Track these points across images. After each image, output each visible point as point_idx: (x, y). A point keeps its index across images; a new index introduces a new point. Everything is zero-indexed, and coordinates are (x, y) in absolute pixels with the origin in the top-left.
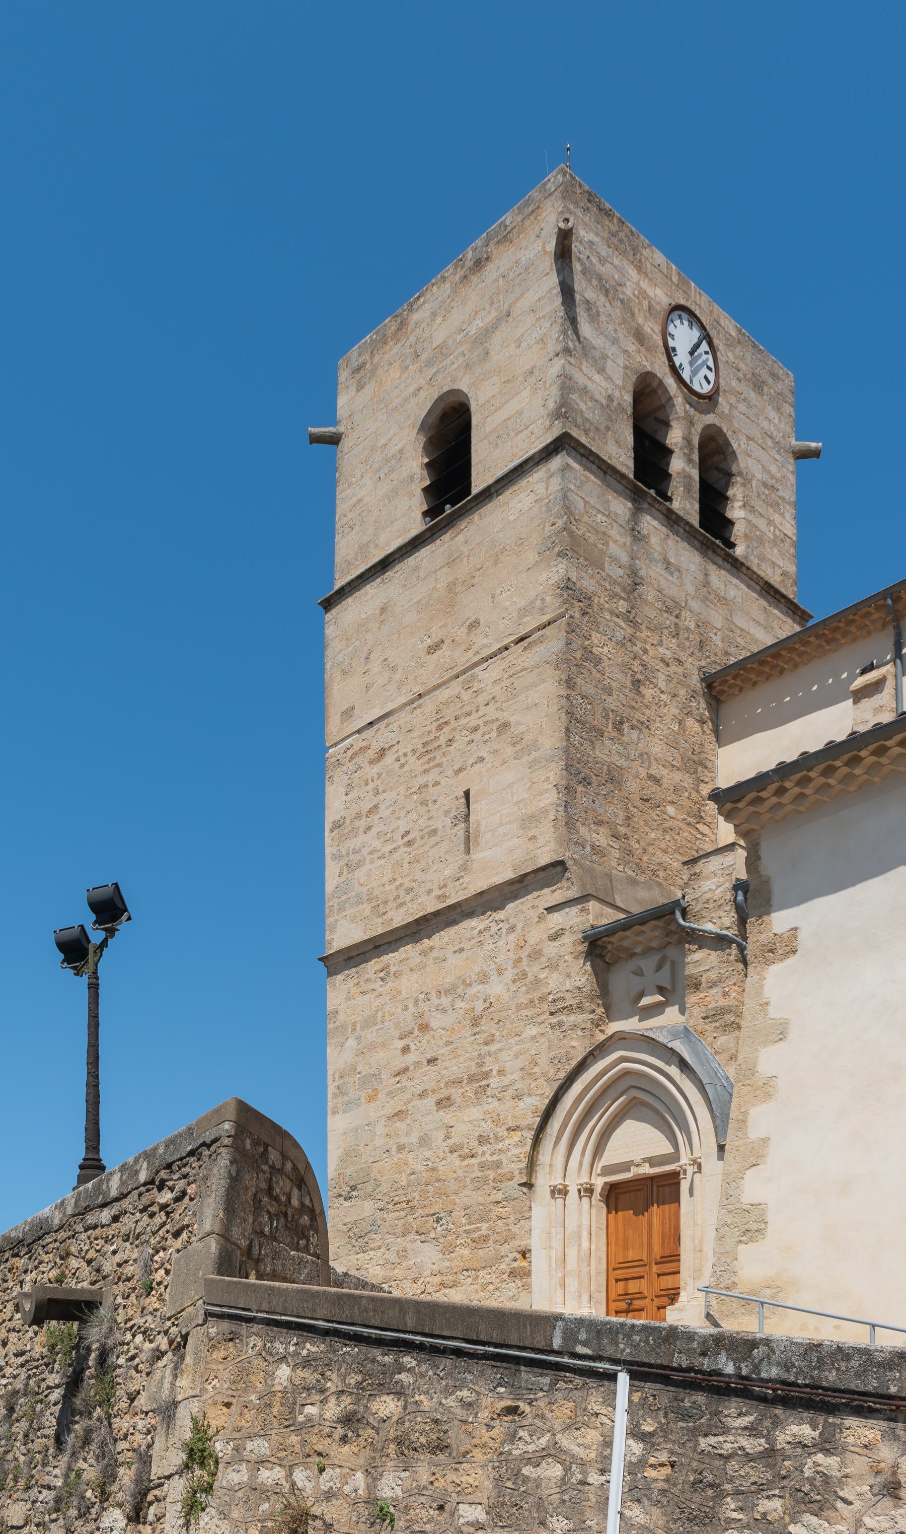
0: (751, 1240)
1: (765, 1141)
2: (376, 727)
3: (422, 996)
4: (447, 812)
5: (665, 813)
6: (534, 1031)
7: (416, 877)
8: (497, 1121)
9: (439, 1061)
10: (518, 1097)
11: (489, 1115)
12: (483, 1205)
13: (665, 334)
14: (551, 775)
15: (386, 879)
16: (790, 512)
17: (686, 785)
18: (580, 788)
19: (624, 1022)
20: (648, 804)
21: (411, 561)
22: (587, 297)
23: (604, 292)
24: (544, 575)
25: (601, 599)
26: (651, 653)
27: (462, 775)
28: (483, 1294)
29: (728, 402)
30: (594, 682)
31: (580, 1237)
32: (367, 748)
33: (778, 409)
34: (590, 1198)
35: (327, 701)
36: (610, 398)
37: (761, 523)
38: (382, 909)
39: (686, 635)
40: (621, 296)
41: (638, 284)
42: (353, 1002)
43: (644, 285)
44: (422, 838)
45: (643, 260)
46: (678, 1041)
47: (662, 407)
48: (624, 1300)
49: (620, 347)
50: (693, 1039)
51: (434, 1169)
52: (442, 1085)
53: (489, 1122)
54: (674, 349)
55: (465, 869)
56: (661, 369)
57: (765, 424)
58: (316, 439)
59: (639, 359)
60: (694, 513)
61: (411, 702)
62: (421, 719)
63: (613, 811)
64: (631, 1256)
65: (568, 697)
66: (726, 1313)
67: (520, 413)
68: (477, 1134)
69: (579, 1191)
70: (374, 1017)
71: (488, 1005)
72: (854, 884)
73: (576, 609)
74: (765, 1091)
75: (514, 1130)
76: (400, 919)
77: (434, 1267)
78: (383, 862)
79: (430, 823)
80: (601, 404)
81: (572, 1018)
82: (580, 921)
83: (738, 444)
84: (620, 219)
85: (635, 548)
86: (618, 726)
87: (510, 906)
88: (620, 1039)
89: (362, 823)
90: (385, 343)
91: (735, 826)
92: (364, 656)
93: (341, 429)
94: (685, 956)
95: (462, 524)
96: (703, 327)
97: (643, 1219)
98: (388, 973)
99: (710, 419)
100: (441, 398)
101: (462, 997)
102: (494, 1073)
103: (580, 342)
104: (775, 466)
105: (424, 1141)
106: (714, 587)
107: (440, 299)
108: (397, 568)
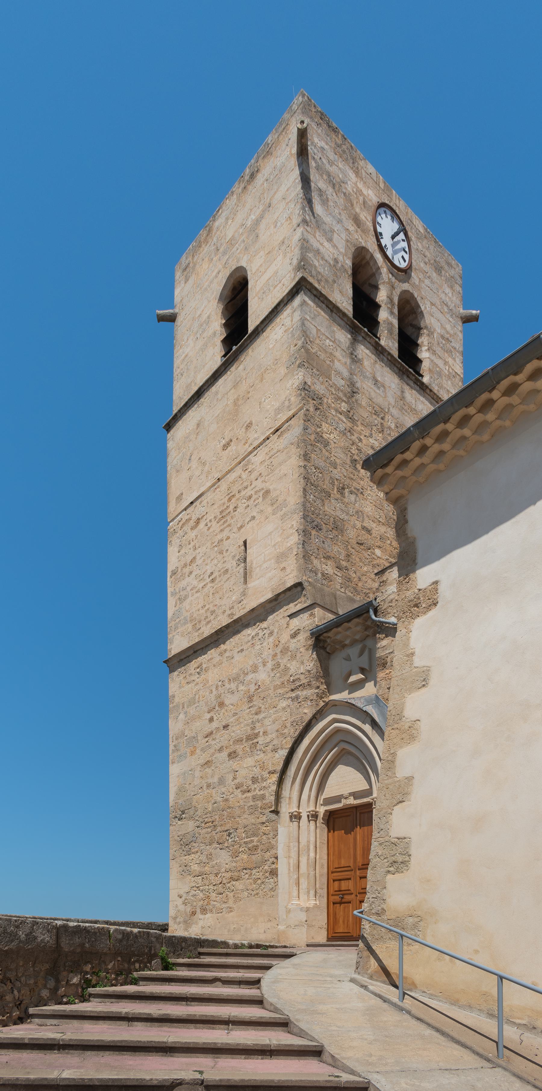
0: (398, 871)
1: (410, 779)
2: (194, 504)
3: (220, 683)
4: (234, 556)
5: (374, 554)
6: (284, 704)
7: (217, 603)
8: (262, 768)
9: (230, 727)
10: (275, 750)
11: (258, 763)
12: (255, 824)
13: (375, 223)
14: (294, 523)
15: (200, 606)
16: (459, 359)
17: (389, 536)
18: (314, 532)
19: (339, 694)
20: (362, 547)
21: (214, 389)
22: (320, 186)
23: (332, 185)
24: (290, 382)
25: (328, 400)
26: (364, 441)
27: (243, 530)
28: (255, 886)
29: (418, 277)
30: (324, 458)
31: (309, 850)
32: (190, 519)
33: (451, 287)
34: (316, 821)
35: (168, 492)
36: (336, 260)
37: (440, 363)
38: (198, 626)
39: (388, 432)
40: (344, 191)
41: (356, 184)
42: (183, 689)
43: (360, 185)
44: (220, 576)
45: (360, 168)
46: (371, 706)
47: (373, 275)
48: (339, 895)
49: (343, 226)
50: (382, 704)
51: (227, 800)
52: (231, 743)
53: (258, 768)
54: (381, 234)
55: (244, 595)
56: (372, 246)
57: (443, 296)
58: (162, 319)
59: (357, 237)
60: (395, 350)
61: (213, 485)
62: (218, 496)
63: (338, 550)
64: (343, 863)
65: (305, 467)
66: (377, 937)
67: (276, 272)
68: (251, 776)
69: (308, 816)
70: (194, 698)
71: (257, 687)
72: (487, 532)
73: (311, 405)
74: (410, 734)
75: (273, 773)
76: (207, 632)
77: (227, 866)
78: (198, 594)
79: (224, 565)
80: (330, 264)
81: (305, 692)
82: (307, 622)
83: (425, 307)
84: (343, 136)
85: (353, 367)
86: (341, 490)
87: (271, 617)
88: (333, 706)
89: (187, 570)
90: (200, 247)
91: (387, 494)
92: (188, 458)
93: (176, 310)
94: (376, 643)
95: (242, 358)
96: (401, 223)
97: (351, 836)
98: (201, 670)
99: (406, 286)
100: (231, 275)
101: (242, 683)
102: (261, 733)
103: (314, 217)
104: (449, 326)
105: (222, 781)
106: (408, 401)
107: (230, 207)
108: (206, 395)
